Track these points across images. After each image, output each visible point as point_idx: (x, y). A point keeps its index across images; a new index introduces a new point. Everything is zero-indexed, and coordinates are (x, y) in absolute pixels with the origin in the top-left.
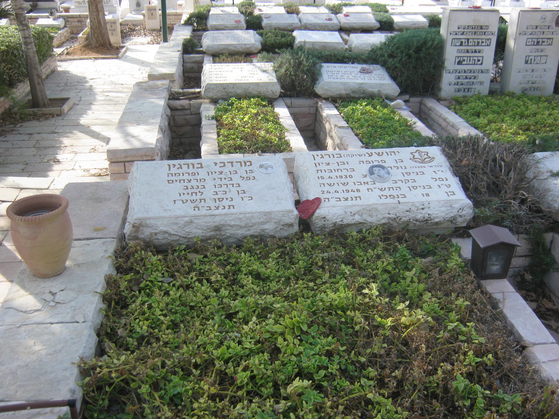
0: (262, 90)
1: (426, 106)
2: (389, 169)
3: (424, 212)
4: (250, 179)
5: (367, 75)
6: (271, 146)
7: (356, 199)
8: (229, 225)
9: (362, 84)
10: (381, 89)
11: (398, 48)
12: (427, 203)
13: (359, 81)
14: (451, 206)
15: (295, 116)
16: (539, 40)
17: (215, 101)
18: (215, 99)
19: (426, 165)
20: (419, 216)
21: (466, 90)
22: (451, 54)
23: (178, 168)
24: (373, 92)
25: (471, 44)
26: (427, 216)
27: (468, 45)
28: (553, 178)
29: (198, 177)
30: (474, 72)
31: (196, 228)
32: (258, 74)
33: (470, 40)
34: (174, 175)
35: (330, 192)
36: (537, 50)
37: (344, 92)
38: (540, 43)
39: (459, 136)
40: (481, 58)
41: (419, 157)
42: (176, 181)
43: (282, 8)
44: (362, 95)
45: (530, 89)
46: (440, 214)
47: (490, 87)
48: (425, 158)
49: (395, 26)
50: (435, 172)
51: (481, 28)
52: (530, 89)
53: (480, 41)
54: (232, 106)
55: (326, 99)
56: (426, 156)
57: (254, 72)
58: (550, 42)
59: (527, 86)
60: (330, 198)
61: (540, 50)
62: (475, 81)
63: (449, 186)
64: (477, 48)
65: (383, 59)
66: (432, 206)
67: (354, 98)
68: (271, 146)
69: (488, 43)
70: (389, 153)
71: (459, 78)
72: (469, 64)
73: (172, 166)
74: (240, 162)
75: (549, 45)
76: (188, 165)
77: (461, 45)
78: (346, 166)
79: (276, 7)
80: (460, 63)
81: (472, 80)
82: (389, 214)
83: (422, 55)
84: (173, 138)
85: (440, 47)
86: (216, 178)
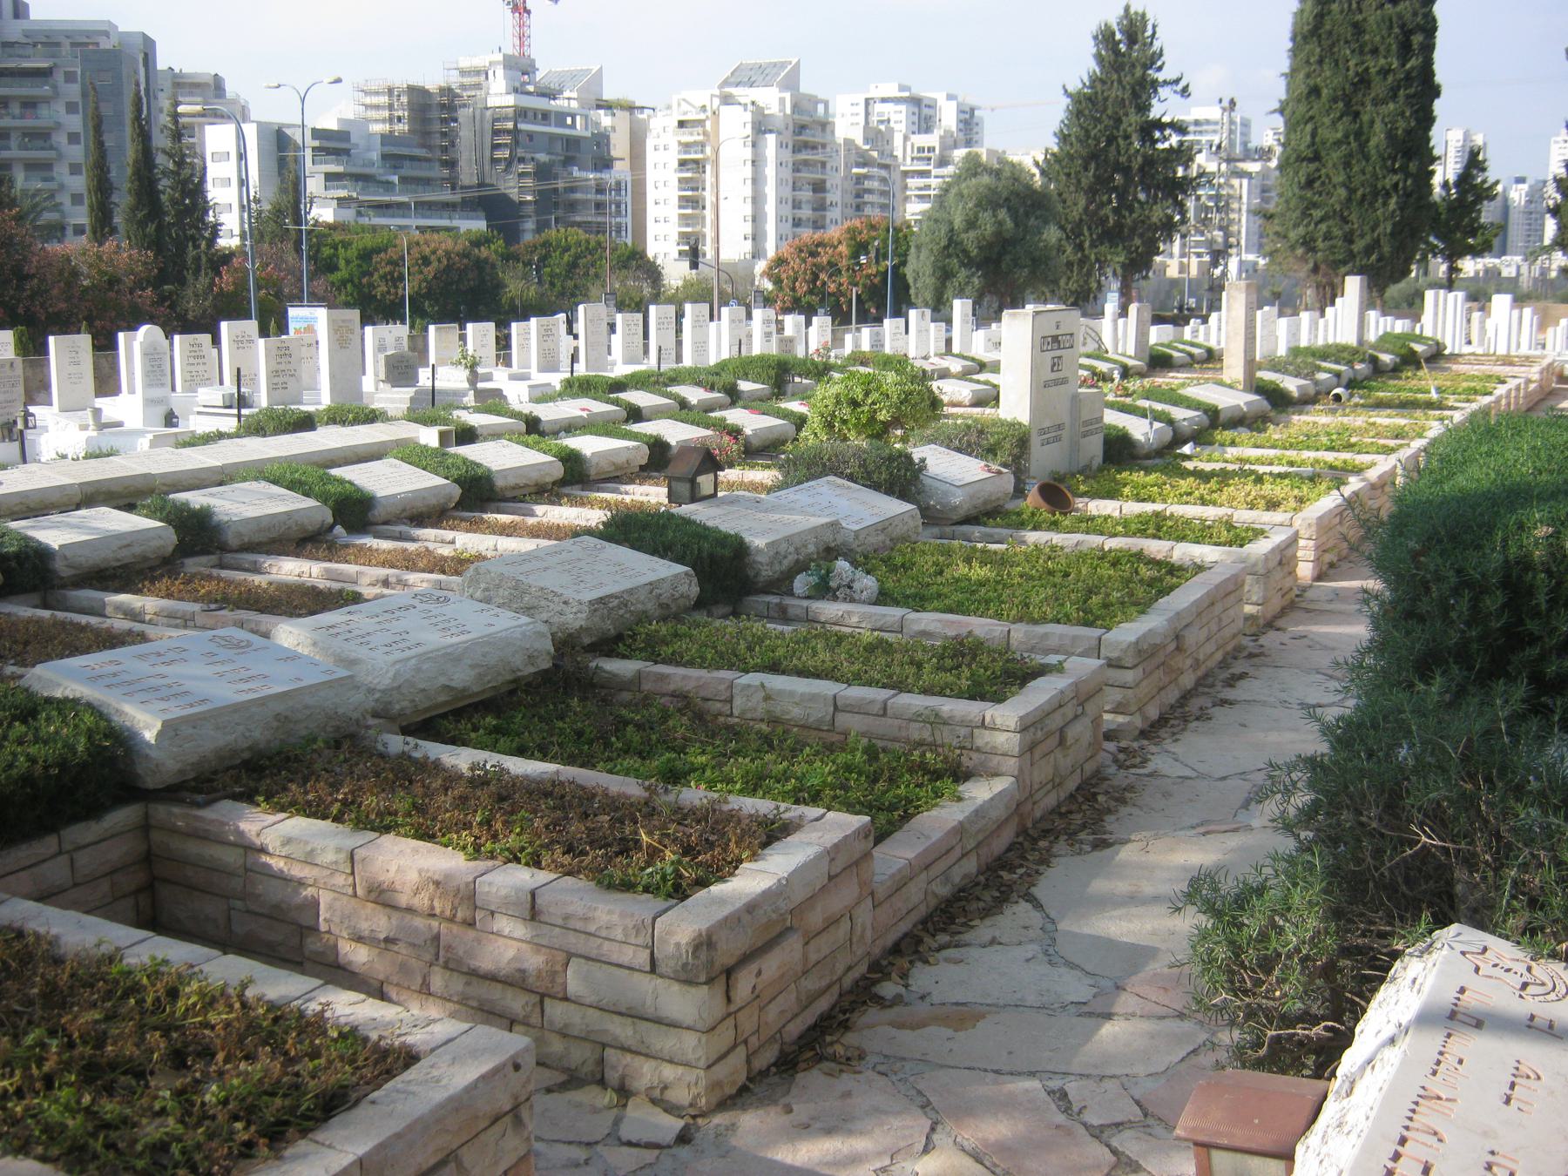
49: (59, 565)
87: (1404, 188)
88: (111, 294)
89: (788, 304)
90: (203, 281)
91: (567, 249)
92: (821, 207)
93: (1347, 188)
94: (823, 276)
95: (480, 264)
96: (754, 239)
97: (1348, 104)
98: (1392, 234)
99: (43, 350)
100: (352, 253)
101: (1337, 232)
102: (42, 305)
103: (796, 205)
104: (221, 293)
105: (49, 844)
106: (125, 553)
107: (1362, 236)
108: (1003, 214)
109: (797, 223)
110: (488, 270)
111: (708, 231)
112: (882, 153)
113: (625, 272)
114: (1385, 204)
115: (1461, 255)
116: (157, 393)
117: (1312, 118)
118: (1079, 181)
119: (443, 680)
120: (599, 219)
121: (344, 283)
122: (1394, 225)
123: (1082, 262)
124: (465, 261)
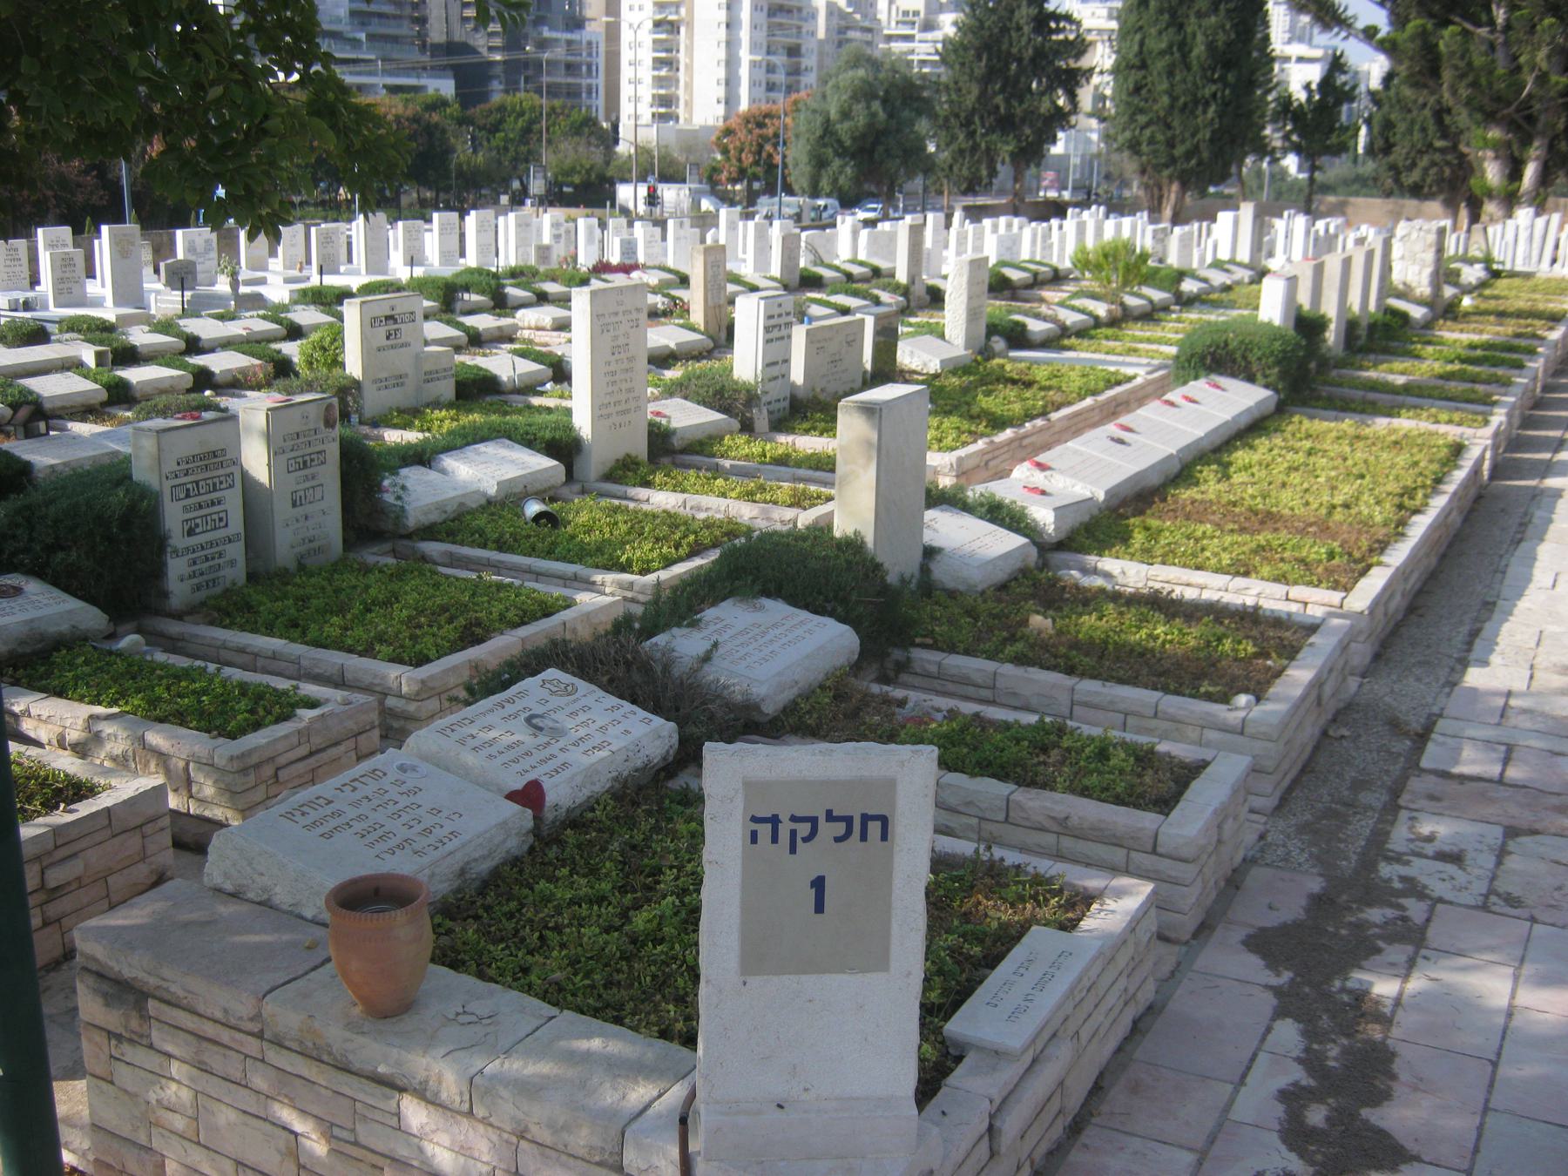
8: (476, 860)
9: (32, 621)
20: (639, 764)
22: (173, 516)
31: (441, 882)
39: (837, 534)
40: (223, 515)
80: (191, 532)
81: (216, 561)
87: (1223, 96)
89: (734, 175)
91: (522, 114)
92: (795, 71)
93: (1170, 96)
94: (768, 148)
95: (430, 130)
96: (727, 103)
97: (1173, 14)
98: (1212, 140)
101: (1160, 137)
103: (771, 69)
107: (1183, 141)
108: (876, 105)
109: (771, 87)
110: (438, 134)
111: (681, 93)
112: (865, 16)
113: (577, 139)
114: (1205, 112)
115: (1320, 154)
117: (1141, 28)
118: (972, 70)
120: (570, 80)
122: (1213, 132)
123: (975, 148)
124: (415, 126)
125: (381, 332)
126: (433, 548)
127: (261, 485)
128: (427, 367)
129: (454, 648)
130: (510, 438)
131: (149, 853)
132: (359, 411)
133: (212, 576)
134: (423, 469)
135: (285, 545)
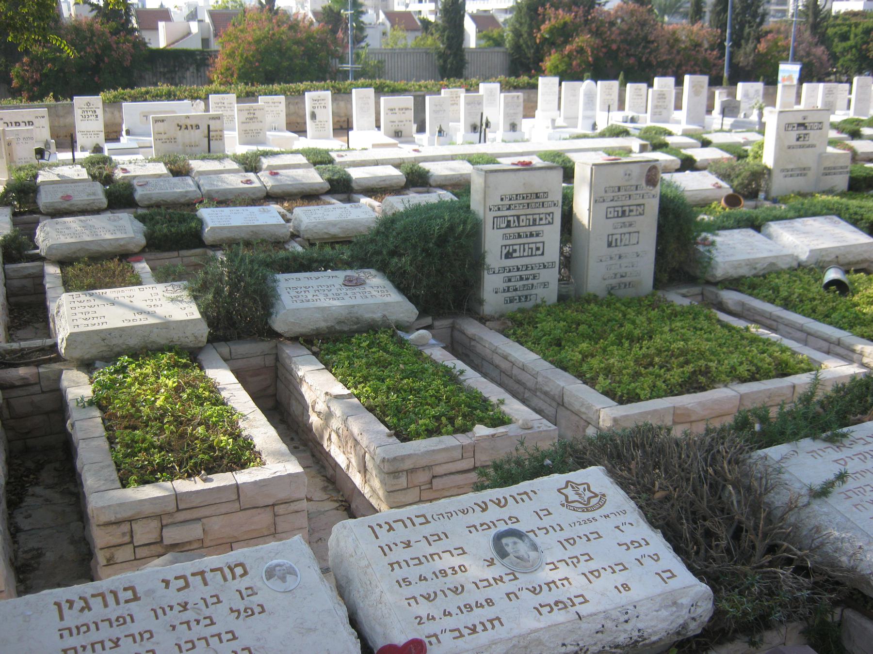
0: (176, 336)
1: (464, 334)
2: (531, 535)
3: (628, 627)
4: (253, 614)
5: (357, 290)
6: (222, 457)
7: (493, 627)
9: (353, 306)
10: (386, 313)
11: (405, 240)
12: (632, 608)
13: (348, 302)
14: (675, 603)
15: (240, 375)
16: (624, 208)
17: (87, 366)
18: (88, 359)
19: (596, 514)
20: (622, 638)
21: (523, 299)
22: (493, 242)
23: (82, 610)
24: (373, 320)
25: (524, 224)
26: (637, 633)
27: (519, 226)
28: (818, 501)
29: (135, 628)
30: (532, 268)
32: (160, 303)
33: (521, 218)
34: (75, 631)
35: (433, 618)
36: (624, 225)
37: (323, 325)
38: (627, 213)
40: (540, 245)
41: (577, 498)
42: (84, 648)
43: (162, 165)
44: (355, 327)
45: (620, 286)
46: (660, 626)
47: (559, 291)
48: (589, 499)
49: (354, 185)
50: (617, 527)
51: (537, 197)
52: (620, 286)
53: (537, 217)
54: (124, 372)
55: (295, 339)
56: (588, 494)
57: (154, 302)
58: (640, 210)
59: (614, 282)
60: (439, 633)
61: (627, 224)
62: (535, 282)
63: (656, 558)
64: (534, 229)
65: (380, 258)
66: (641, 610)
67: (342, 332)
68: (222, 457)
69: (550, 219)
70: (518, 498)
71: (510, 280)
72: (523, 256)
73: (65, 606)
74: (220, 569)
75: (640, 214)
76: (102, 595)
77: (508, 226)
78: (444, 544)
79: (151, 164)
80: (508, 256)
81: (530, 281)
82: (564, 645)
83: (450, 249)
84: (9, 441)
85: (475, 232)
86: (176, 623)
88: (693, 52)
90: (750, 46)
99: (625, 86)
100: (860, 29)
102: (655, 57)
104: (759, 54)
105: (175, 254)
106: (382, 183)
116: (589, 113)
119: (325, 231)
121: (851, 48)
125: (794, 134)
126: (730, 297)
127: (583, 226)
128: (828, 164)
129: (672, 392)
130: (839, 216)
131: (279, 529)
132: (767, 192)
133: (525, 293)
134: (751, 232)
135: (596, 275)
